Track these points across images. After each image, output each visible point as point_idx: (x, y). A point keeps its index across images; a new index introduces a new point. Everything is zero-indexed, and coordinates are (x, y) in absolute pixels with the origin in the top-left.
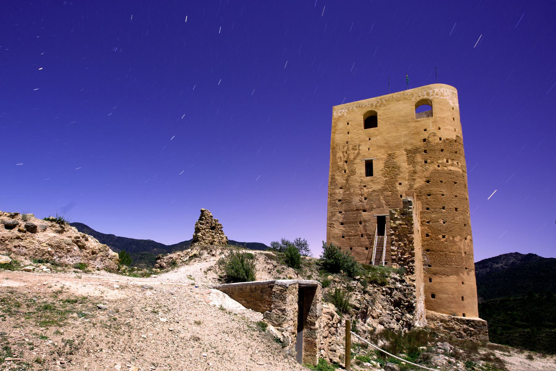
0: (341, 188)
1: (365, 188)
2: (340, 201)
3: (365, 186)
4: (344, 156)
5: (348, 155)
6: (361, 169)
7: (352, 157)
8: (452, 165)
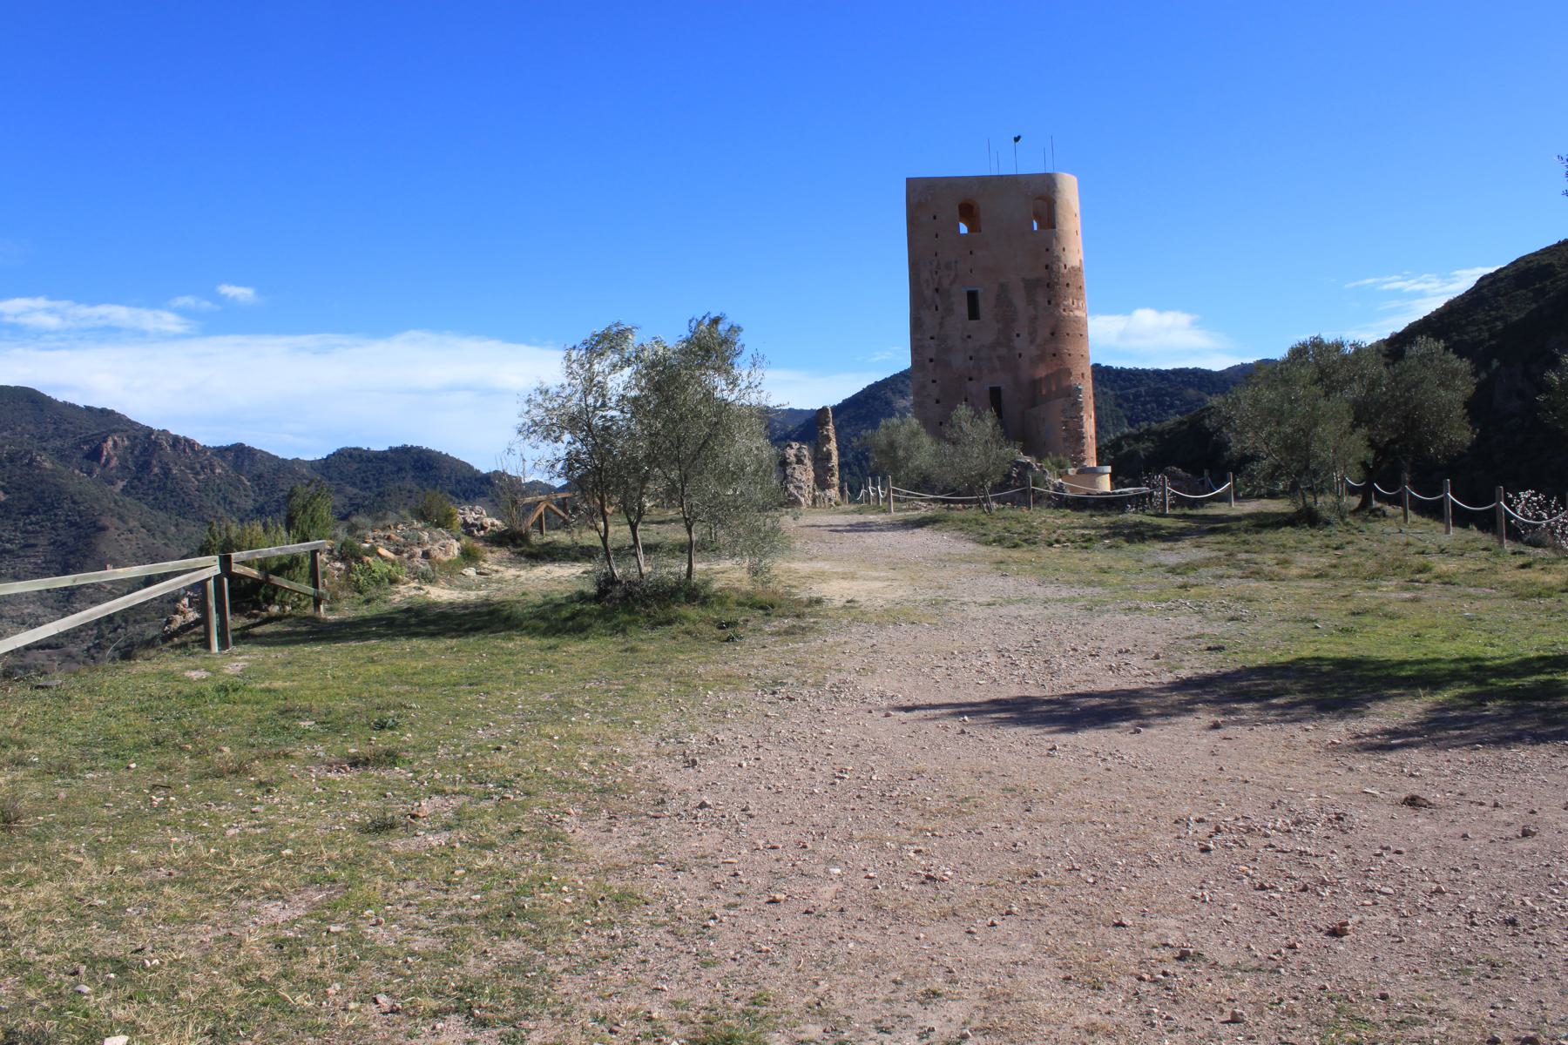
6: (962, 308)
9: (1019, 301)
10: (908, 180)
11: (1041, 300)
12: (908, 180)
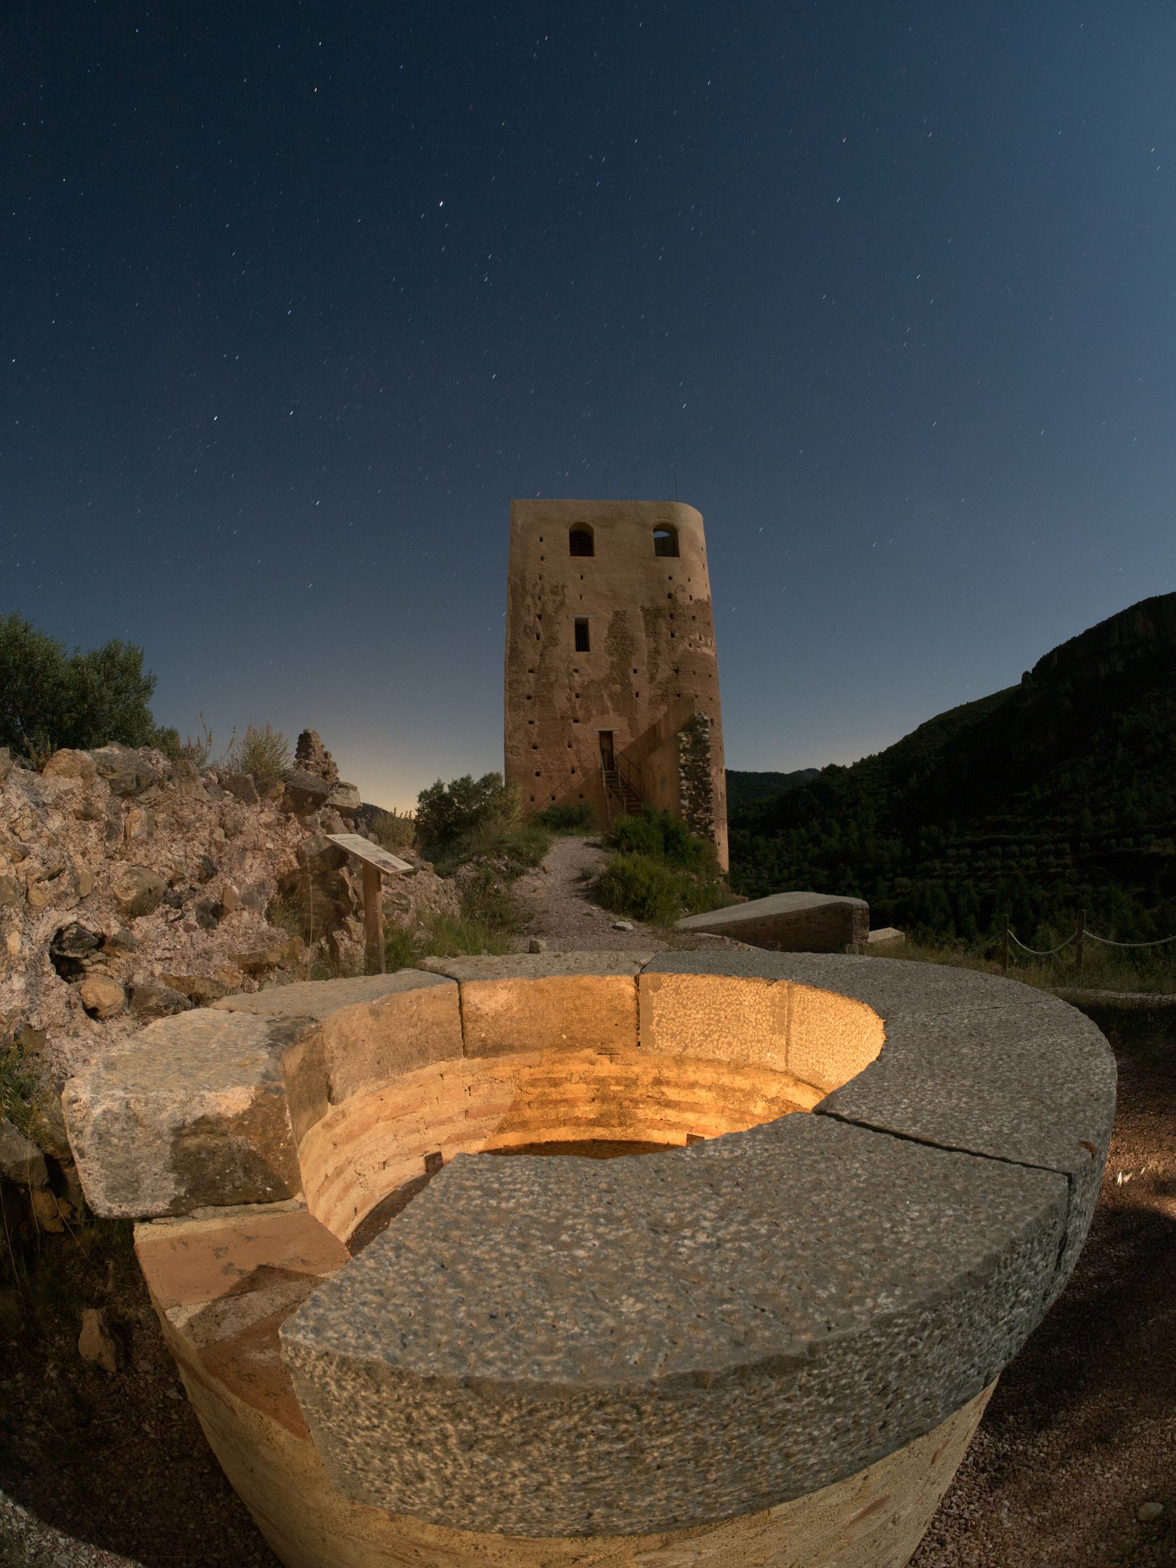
0: (531, 671)
1: (576, 675)
3: (576, 671)
5: (544, 603)
6: (568, 636)
7: (550, 608)
8: (706, 645)
9: (638, 628)
10: (678, 555)
11: (663, 626)
12: (678, 555)
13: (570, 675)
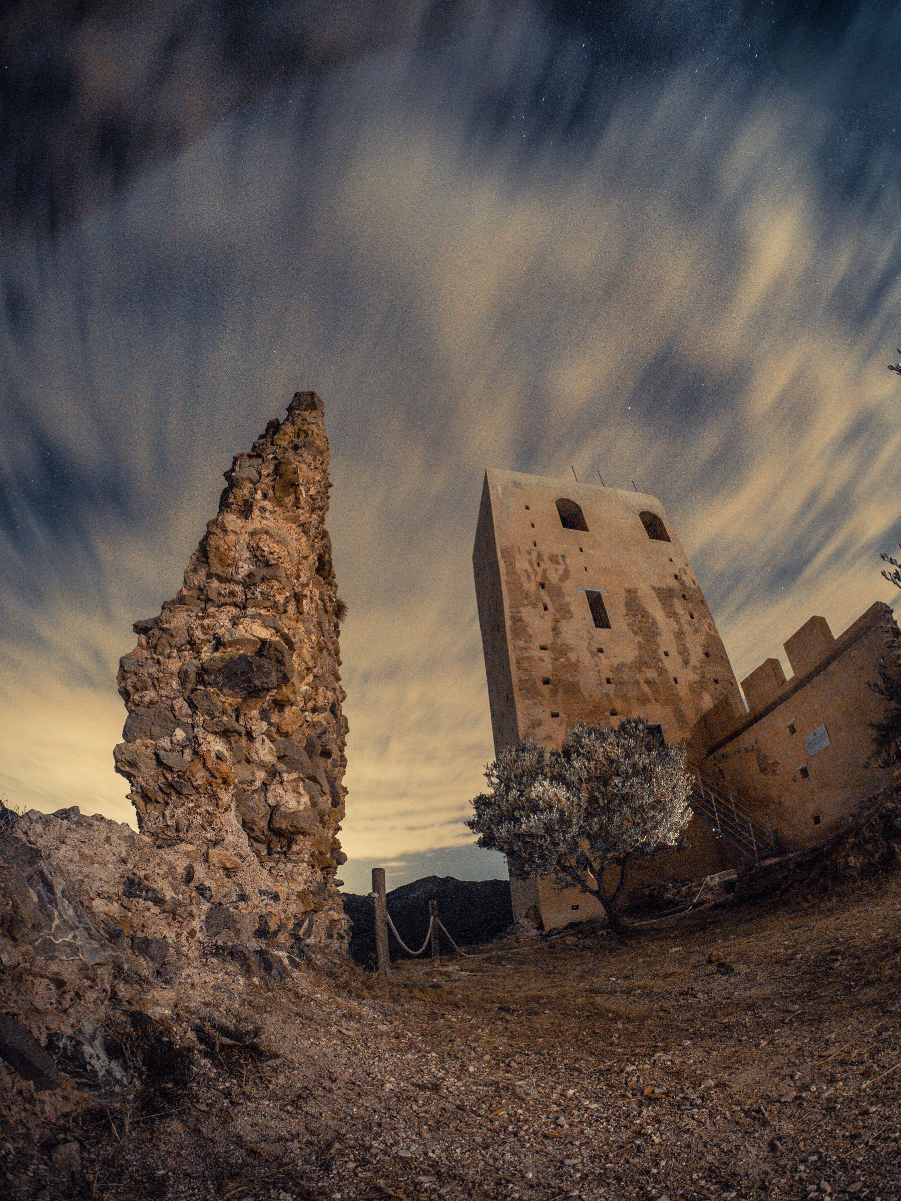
0: (543, 648)
2: (546, 682)
3: (600, 650)
4: (536, 573)
6: (582, 613)
13: (593, 655)
